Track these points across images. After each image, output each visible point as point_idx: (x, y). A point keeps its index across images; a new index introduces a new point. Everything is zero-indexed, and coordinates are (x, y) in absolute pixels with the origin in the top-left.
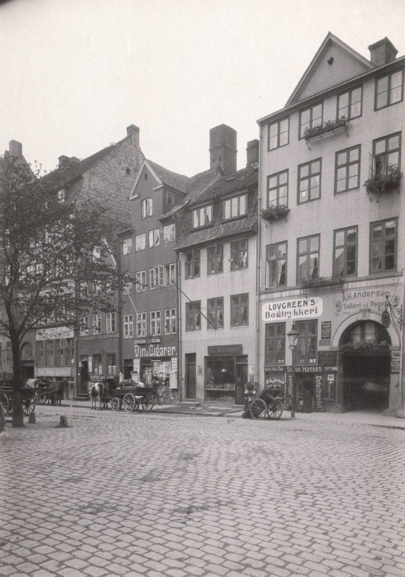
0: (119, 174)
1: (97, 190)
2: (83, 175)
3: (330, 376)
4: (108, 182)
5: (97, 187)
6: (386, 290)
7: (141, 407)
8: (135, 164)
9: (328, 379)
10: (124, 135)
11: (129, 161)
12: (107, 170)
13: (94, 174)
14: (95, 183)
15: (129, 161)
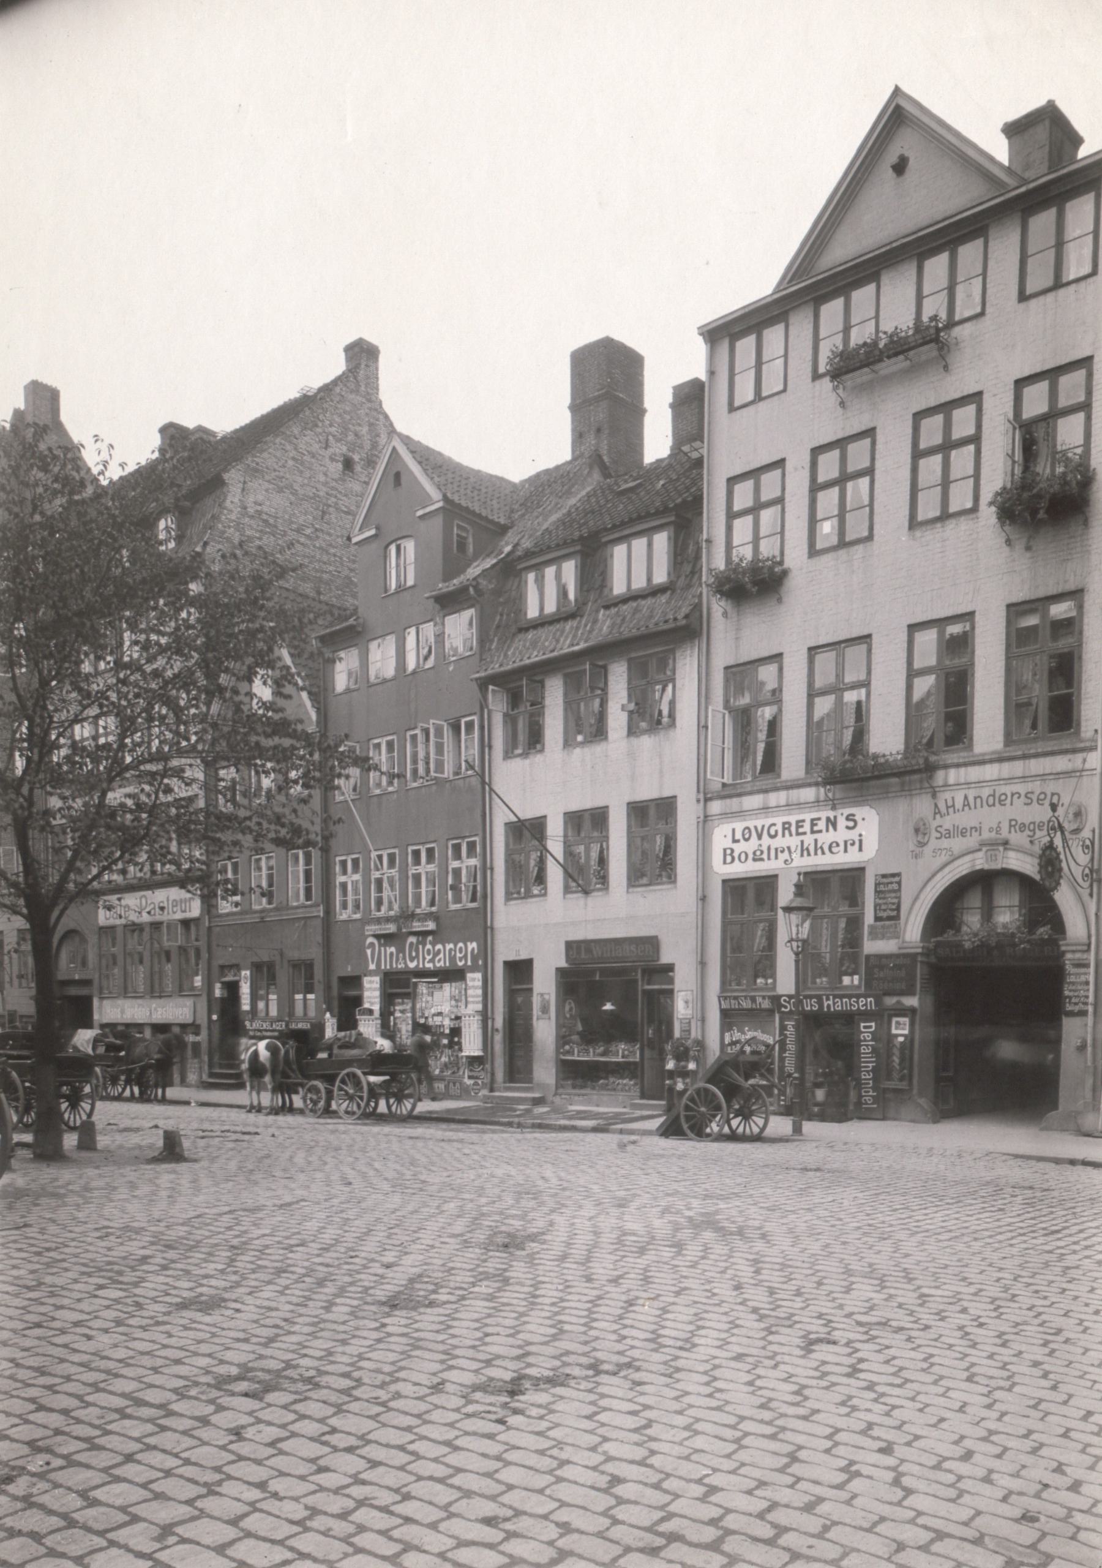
0: (325, 474)
1: (265, 517)
2: (226, 476)
3: (898, 1023)
4: (295, 493)
5: (265, 509)
8: (367, 445)
9: (894, 1031)
10: (337, 366)
11: (351, 437)
12: (291, 463)
13: (255, 472)
14: (260, 498)
15: (351, 437)
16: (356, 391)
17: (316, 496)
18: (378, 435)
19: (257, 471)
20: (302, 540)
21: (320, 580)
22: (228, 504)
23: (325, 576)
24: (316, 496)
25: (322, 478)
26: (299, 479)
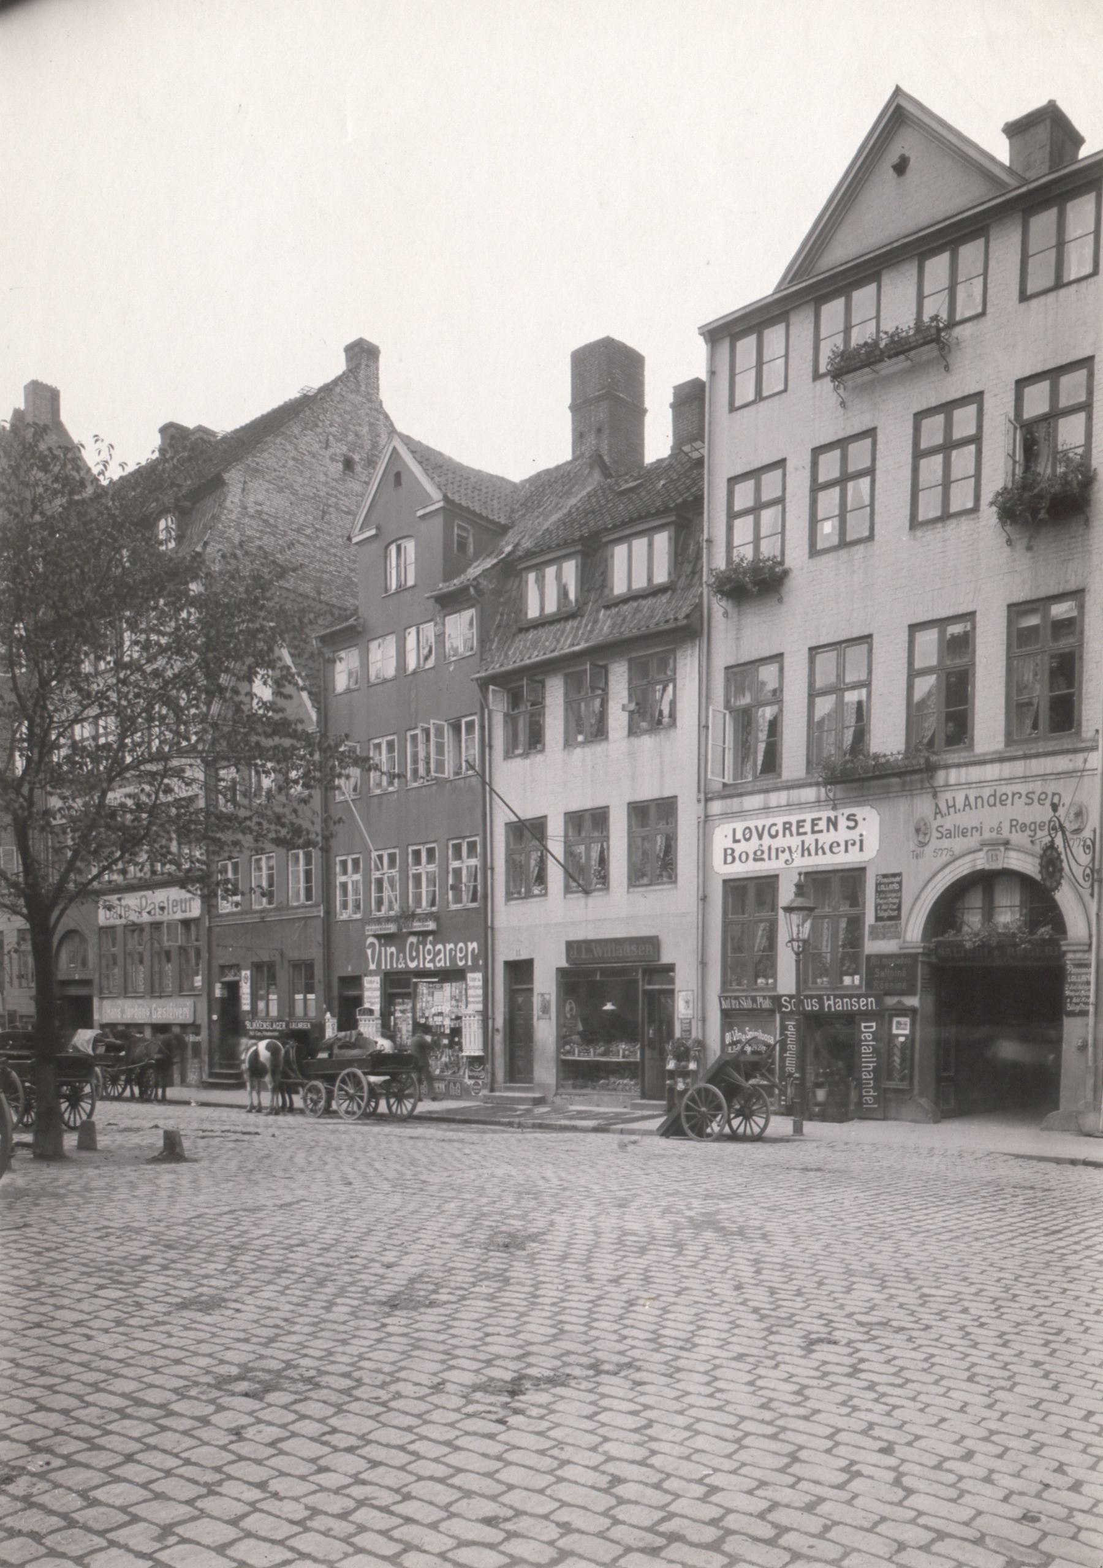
0: (326, 474)
1: (265, 517)
2: (226, 476)
3: (899, 1023)
4: (295, 493)
5: (265, 509)
6: (1052, 787)
7: (383, 1107)
8: (368, 445)
9: (895, 1031)
10: (338, 366)
11: (351, 437)
12: (291, 463)
13: (255, 472)
14: (260, 498)
15: (351, 437)
16: (357, 391)
17: (316, 496)
18: (378, 435)
19: (257, 471)
20: (303, 540)
21: (321, 580)
22: (228, 504)
23: (325, 576)
24: (316, 496)
25: (323, 478)
26: (300, 479)
